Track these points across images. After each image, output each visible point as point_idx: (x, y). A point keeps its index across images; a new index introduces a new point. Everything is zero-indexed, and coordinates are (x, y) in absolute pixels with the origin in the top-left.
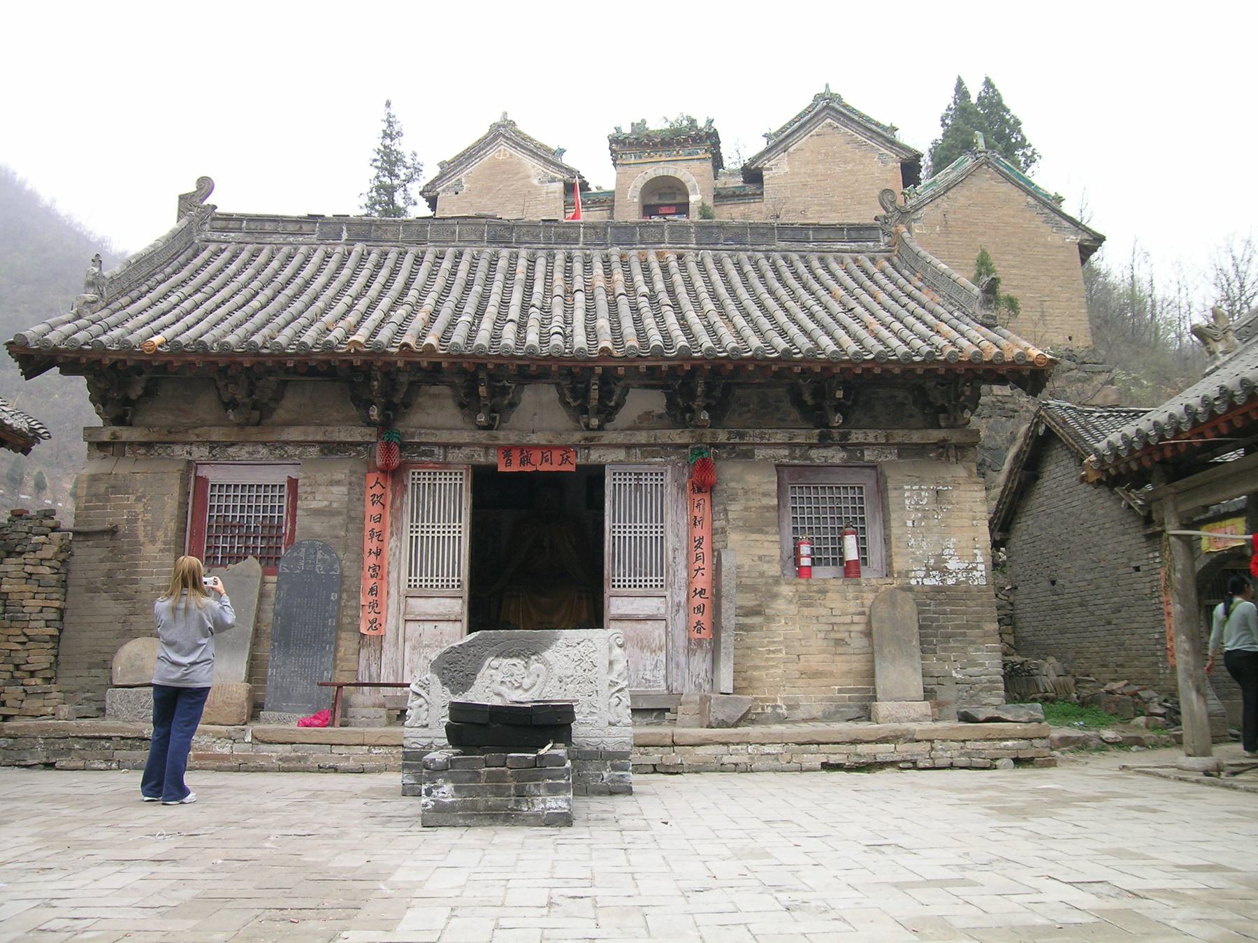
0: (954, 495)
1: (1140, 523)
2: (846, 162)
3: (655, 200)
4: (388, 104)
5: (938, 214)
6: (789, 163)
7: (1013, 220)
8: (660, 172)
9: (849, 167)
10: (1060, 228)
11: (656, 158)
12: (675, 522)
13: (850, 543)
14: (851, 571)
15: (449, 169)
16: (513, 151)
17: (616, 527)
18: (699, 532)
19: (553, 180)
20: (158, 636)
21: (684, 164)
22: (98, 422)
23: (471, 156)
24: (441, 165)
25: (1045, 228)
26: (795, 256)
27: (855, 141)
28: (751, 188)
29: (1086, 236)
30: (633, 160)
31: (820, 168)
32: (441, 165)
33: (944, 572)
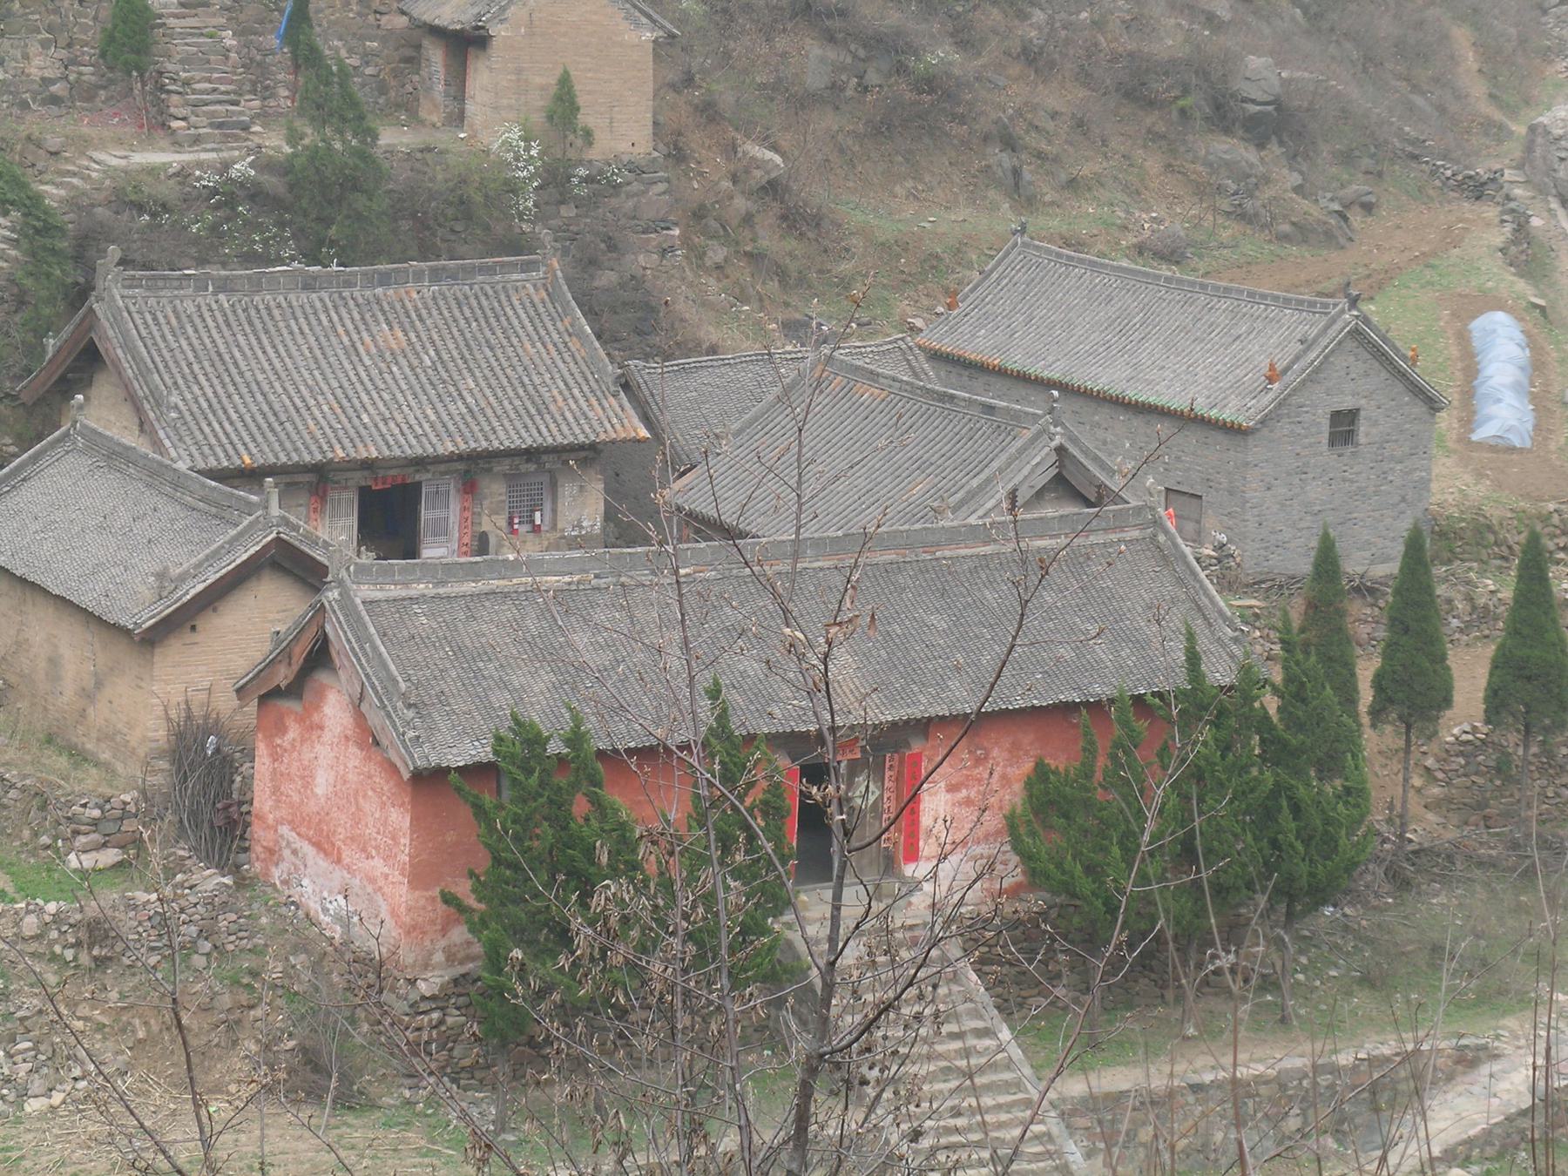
0: (589, 487)
7: (595, 18)
10: (638, 25)
12: (454, 512)
13: (538, 514)
14: (536, 529)
17: (426, 514)
18: (467, 514)
25: (624, 25)
26: (487, 288)
29: (661, 33)
33: (581, 527)
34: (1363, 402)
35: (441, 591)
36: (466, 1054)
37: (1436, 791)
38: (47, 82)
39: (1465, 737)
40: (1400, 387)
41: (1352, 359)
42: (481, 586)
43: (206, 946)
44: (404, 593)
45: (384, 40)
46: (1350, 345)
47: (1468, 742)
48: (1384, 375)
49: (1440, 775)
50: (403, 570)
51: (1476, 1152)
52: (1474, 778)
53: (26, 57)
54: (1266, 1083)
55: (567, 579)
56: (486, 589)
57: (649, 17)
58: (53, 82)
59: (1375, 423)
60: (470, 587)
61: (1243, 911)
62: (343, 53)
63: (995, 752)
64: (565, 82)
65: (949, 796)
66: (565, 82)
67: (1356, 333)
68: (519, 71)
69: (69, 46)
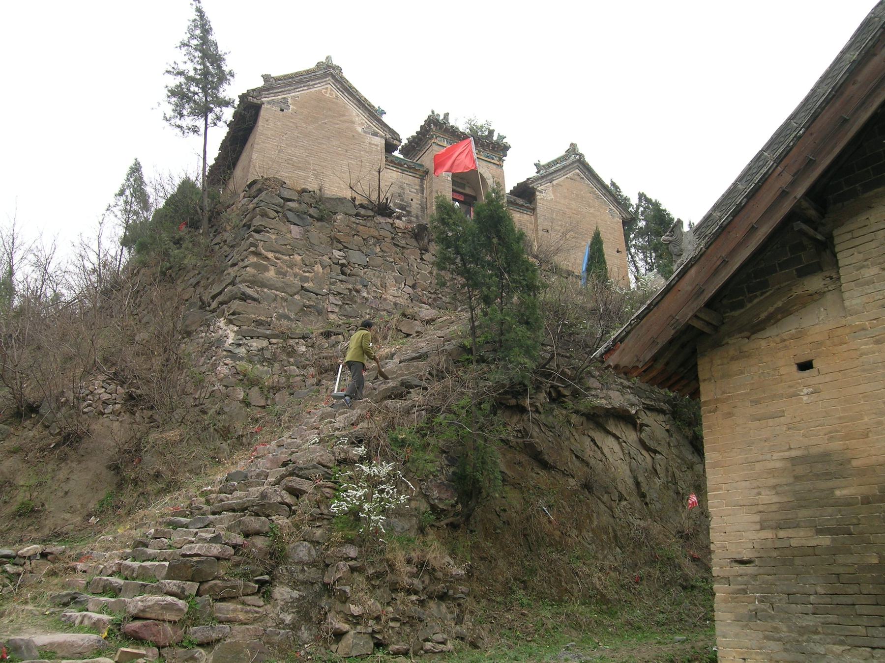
2: (590, 206)
6: (554, 192)
9: (592, 211)
15: (271, 84)
16: (339, 94)
19: (375, 134)
20: (522, 493)
22: (449, 195)
23: (301, 82)
24: (239, 97)
27: (594, 193)
31: (574, 205)
53: (384, 286)
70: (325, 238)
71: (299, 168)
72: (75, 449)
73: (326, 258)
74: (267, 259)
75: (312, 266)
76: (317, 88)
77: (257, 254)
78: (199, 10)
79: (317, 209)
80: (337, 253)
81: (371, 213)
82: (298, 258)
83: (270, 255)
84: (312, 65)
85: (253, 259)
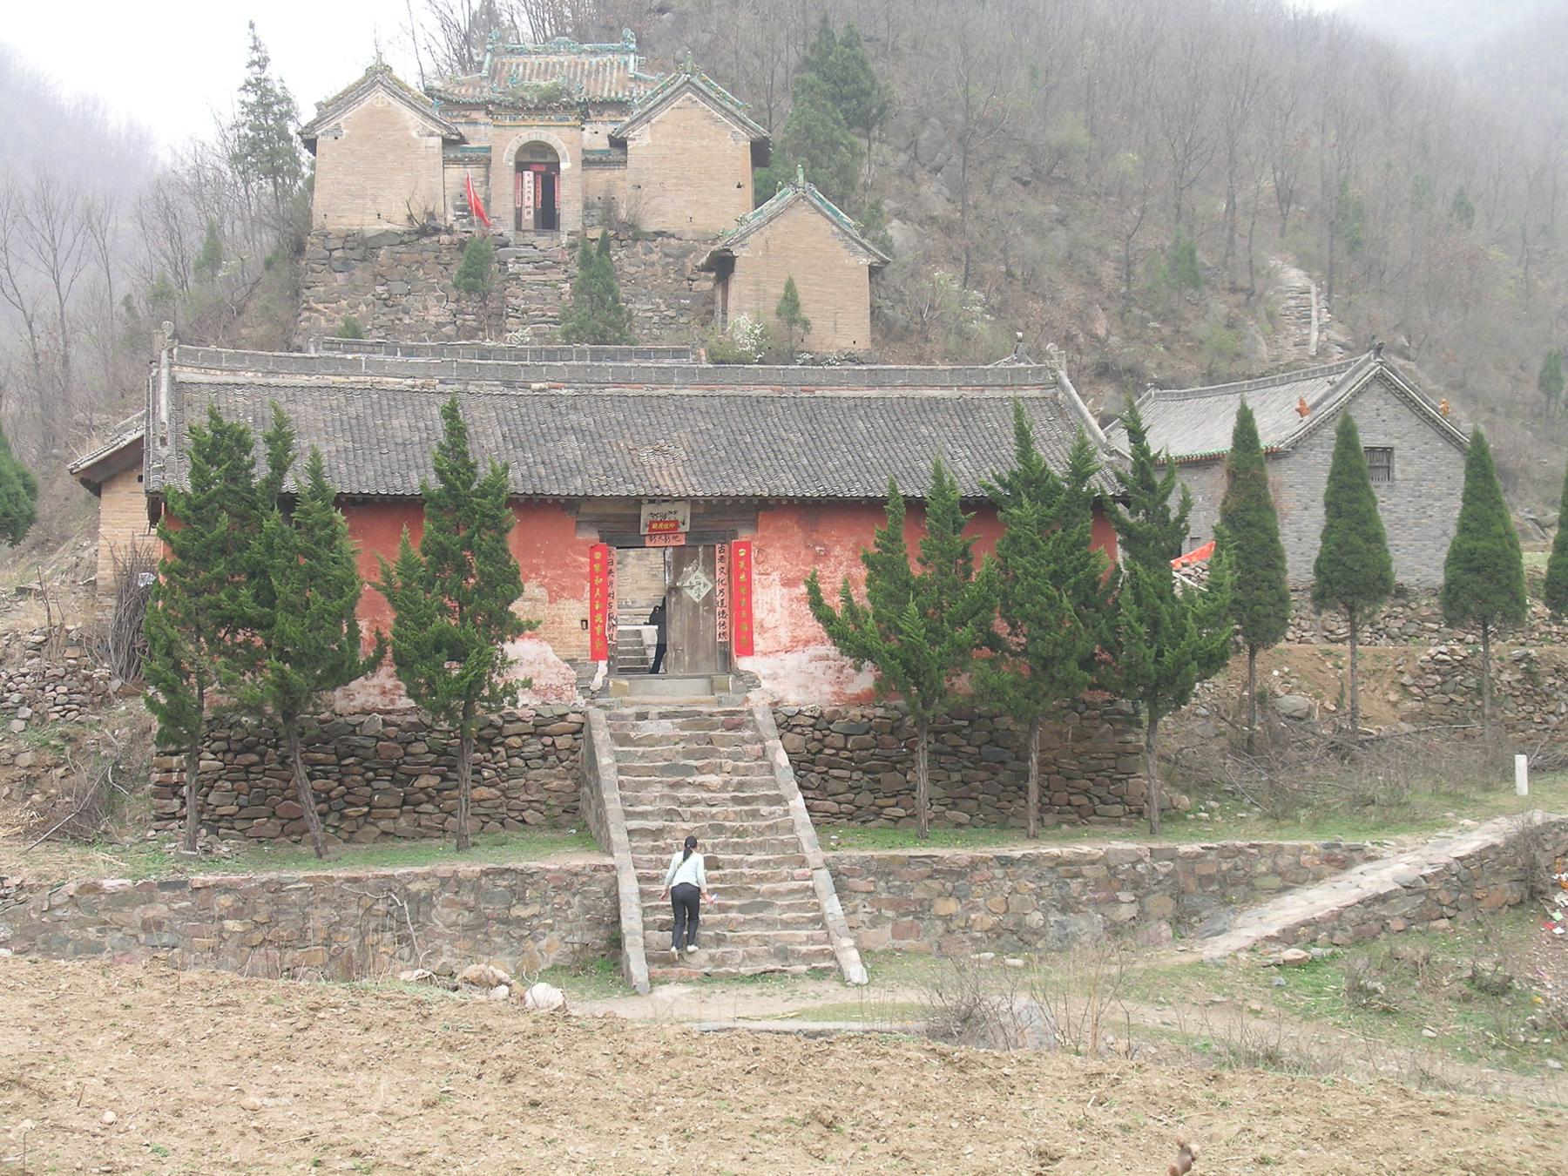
1: (354, 412)
2: (702, 138)
3: (527, 158)
4: (252, 26)
5: (762, 240)
8: (534, 137)
10: (856, 253)
11: (530, 122)
16: (391, 99)
19: (431, 134)
21: (556, 130)
24: (319, 106)
27: (711, 117)
28: (616, 154)
30: (508, 122)
32: (319, 106)
34: (1395, 442)
35: (272, 381)
36: (222, 800)
37: (1409, 704)
38: (439, 325)
39: (1440, 656)
40: (1431, 434)
41: (1381, 402)
42: (314, 380)
43: (28, 712)
44: (231, 379)
45: (693, 298)
46: (1377, 389)
47: (1444, 661)
48: (1415, 420)
49: (1415, 690)
50: (230, 358)
51: (1322, 935)
52: (1452, 696)
53: (426, 308)
54: (1093, 863)
55: (409, 382)
56: (321, 383)
57: (864, 246)
58: (444, 325)
59: (1410, 463)
60: (301, 380)
61: (1130, 738)
62: (663, 307)
63: (837, 550)
64: (790, 286)
65: (785, 591)
66: (790, 286)
67: (1380, 378)
68: (758, 283)
69: (457, 300)
70: (368, 276)
71: (358, 197)
72: (473, 209)
73: (369, 296)
74: (318, 311)
75: (357, 306)
76: (368, 100)
77: (309, 309)
78: (255, 38)
79: (362, 247)
80: (379, 289)
81: (414, 237)
82: (344, 303)
83: (320, 307)
84: (360, 74)
85: (307, 314)
